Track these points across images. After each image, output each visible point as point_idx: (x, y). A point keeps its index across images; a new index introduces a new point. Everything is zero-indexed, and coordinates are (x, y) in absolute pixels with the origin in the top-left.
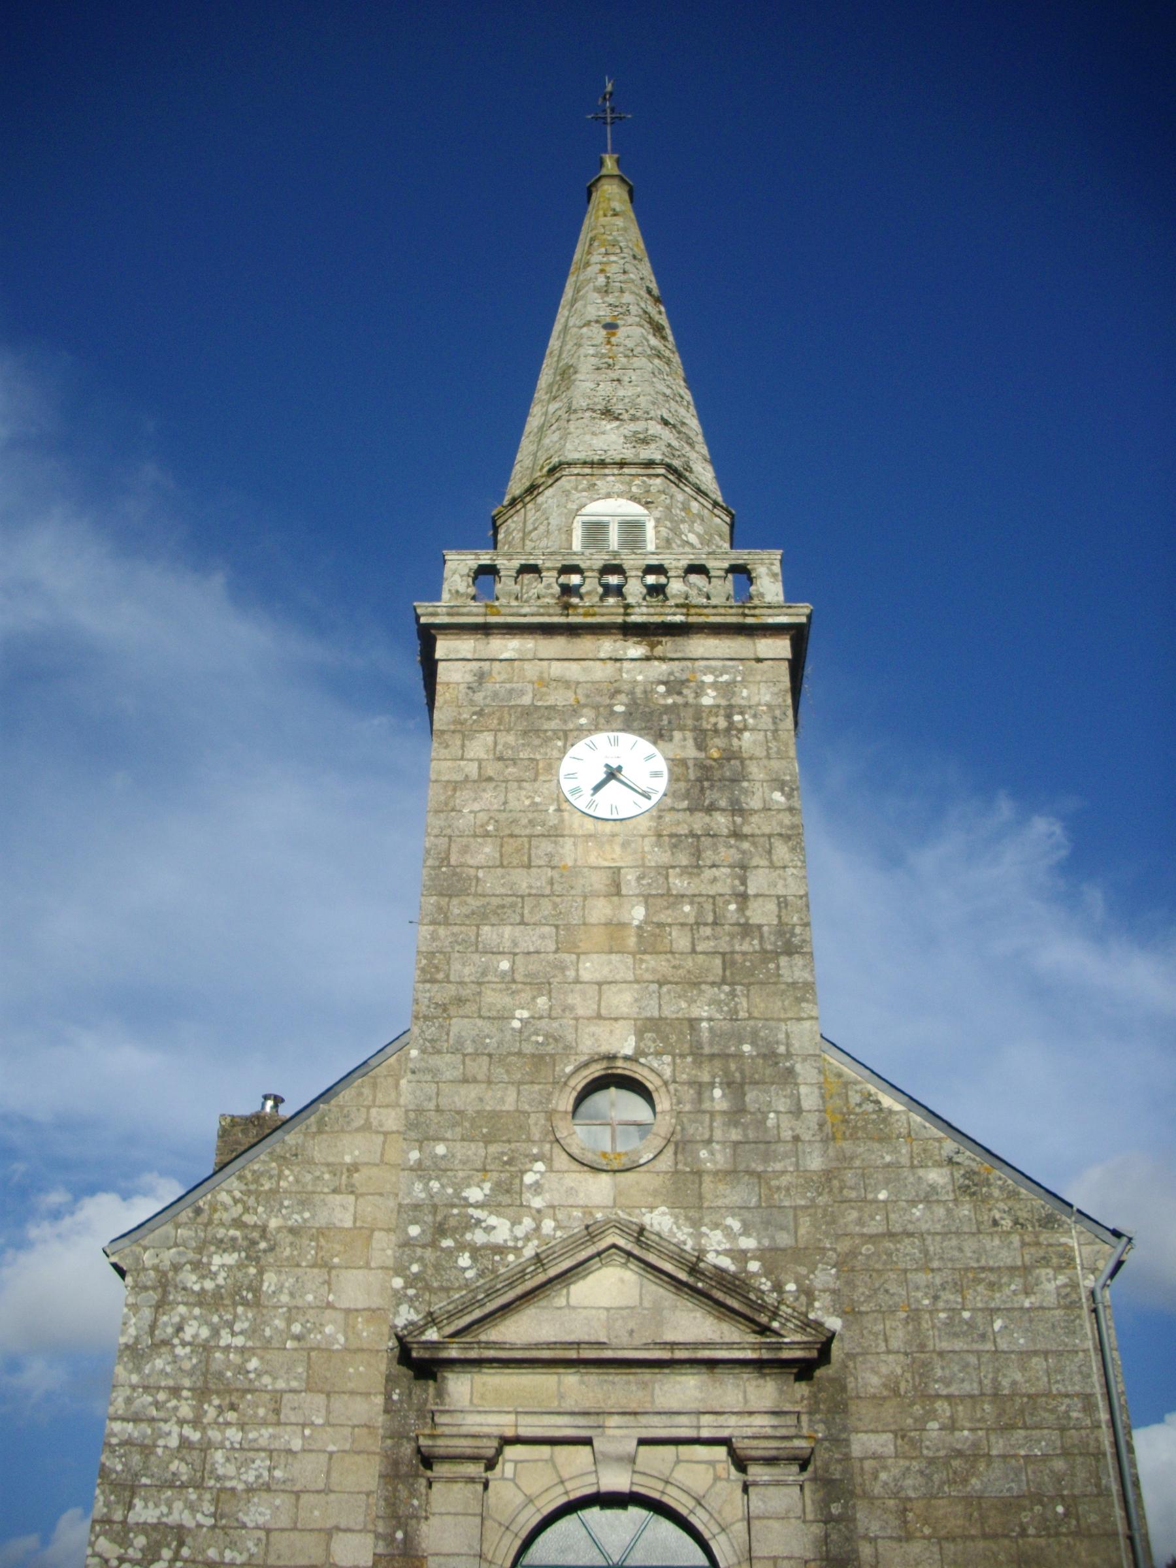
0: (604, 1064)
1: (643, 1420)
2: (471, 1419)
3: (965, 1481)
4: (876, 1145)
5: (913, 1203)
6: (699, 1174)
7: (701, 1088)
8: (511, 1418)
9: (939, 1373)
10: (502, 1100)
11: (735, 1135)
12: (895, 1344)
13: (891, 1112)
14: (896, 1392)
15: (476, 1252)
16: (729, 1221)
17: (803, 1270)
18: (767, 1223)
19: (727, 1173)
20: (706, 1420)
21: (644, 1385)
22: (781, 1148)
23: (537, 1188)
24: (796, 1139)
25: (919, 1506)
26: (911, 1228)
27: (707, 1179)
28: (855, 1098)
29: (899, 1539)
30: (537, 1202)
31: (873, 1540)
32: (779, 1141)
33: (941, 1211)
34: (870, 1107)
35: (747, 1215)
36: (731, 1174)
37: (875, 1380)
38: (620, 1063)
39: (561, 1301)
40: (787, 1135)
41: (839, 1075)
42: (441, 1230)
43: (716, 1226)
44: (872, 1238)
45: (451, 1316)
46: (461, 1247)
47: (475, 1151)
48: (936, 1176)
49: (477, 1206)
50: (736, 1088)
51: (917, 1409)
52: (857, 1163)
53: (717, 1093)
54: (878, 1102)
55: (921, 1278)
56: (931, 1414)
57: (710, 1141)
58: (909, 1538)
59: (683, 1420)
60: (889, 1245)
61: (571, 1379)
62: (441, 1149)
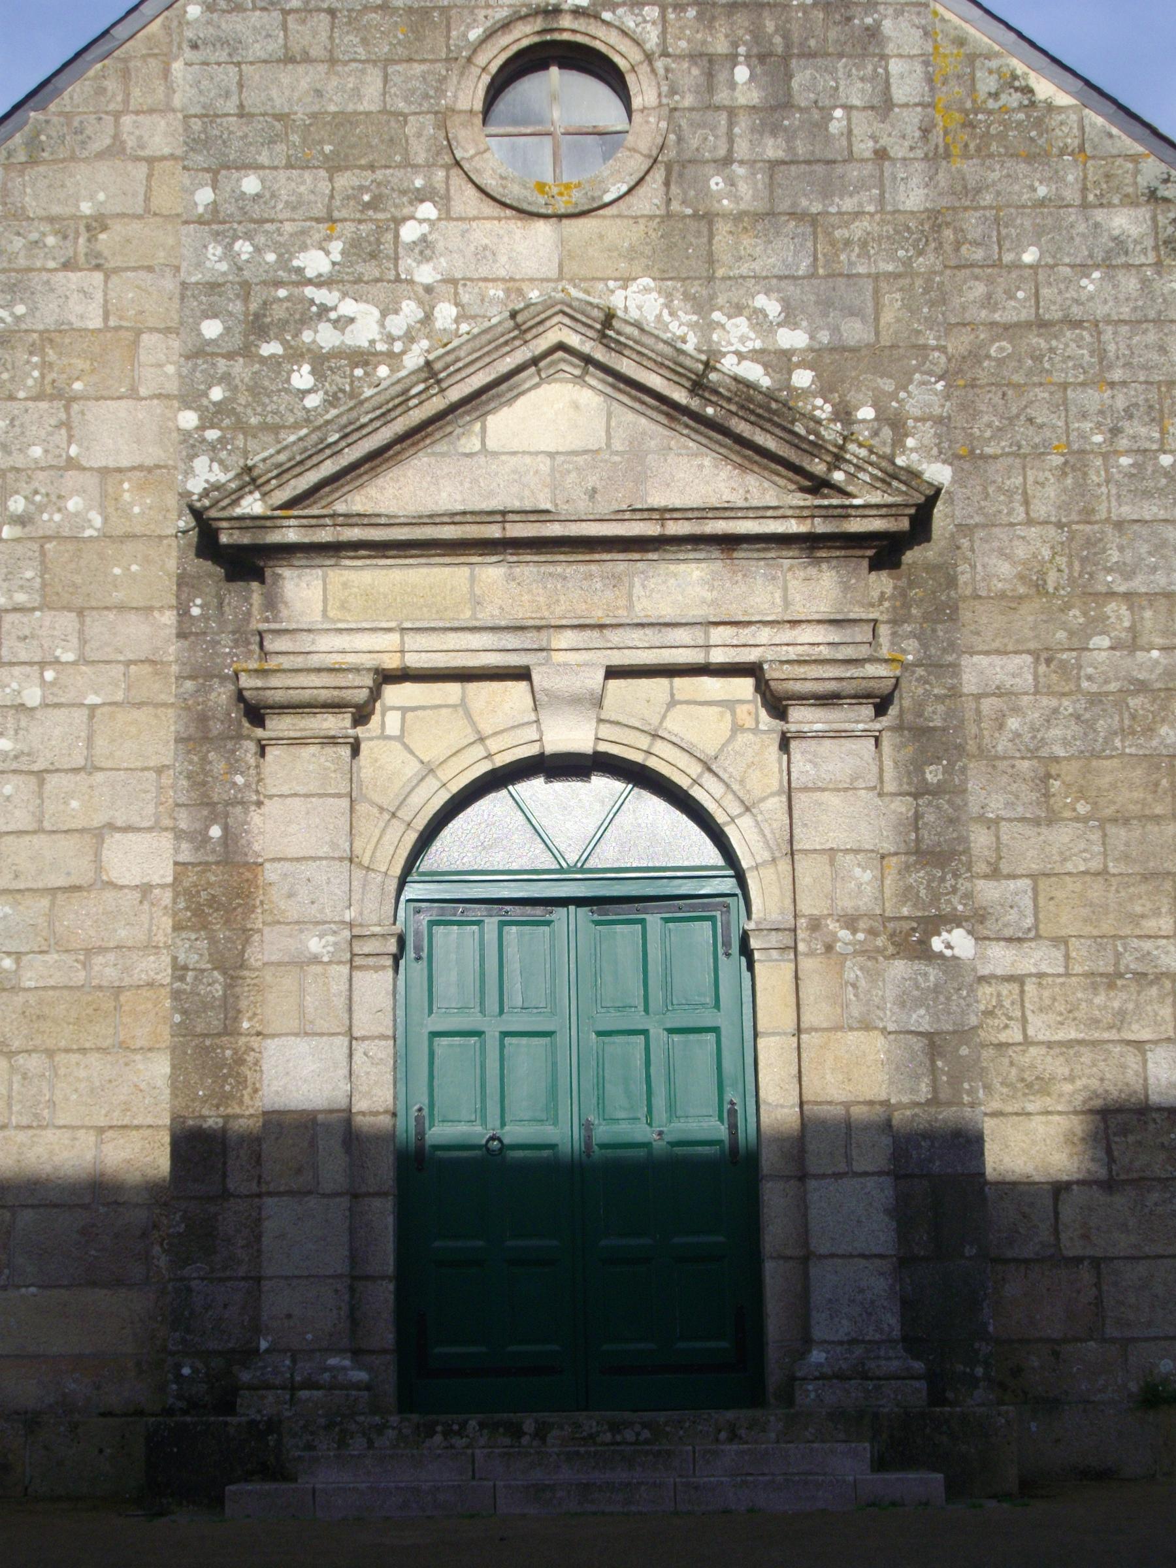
0: (539, 24)
1: (615, 637)
2: (325, 643)
3: (1149, 731)
4: (1022, 168)
5: (1083, 269)
6: (708, 218)
7: (712, 66)
8: (392, 640)
9: (1115, 556)
10: (357, 93)
11: (773, 149)
12: (1041, 510)
13: (1050, 107)
14: (1040, 588)
15: (321, 362)
16: (761, 301)
17: (888, 385)
18: (826, 304)
19: (758, 217)
20: (719, 635)
21: (616, 581)
22: (854, 172)
23: (424, 248)
24: (881, 155)
25: (1069, 771)
26: (1076, 312)
27: (722, 228)
28: (987, 83)
29: (1036, 822)
30: (425, 274)
31: (993, 824)
32: (850, 158)
33: (1130, 284)
34: (1013, 99)
35: (791, 289)
36: (764, 219)
37: (1005, 569)
38: (566, 22)
39: (474, 444)
40: (864, 148)
41: (961, 42)
42: (258, 327)
43: (738, 309)
44: (1008, 330)
45: (284, 473)
46: (296, 355)
47: (312, 185)
48: (1125, 222)
49: (320, 282)
50: (774, 64)
51: (1075, 616)
52: (988, 198)
53: (742, 73)
54: (1028, 91)
55: (1092, 399)
56: (1097, 624)
57: (727, 161)
58: (1052, 819)
59: (681, 635)
60: (1036, 341)
61: (492, 573)
62: (251, 184)
